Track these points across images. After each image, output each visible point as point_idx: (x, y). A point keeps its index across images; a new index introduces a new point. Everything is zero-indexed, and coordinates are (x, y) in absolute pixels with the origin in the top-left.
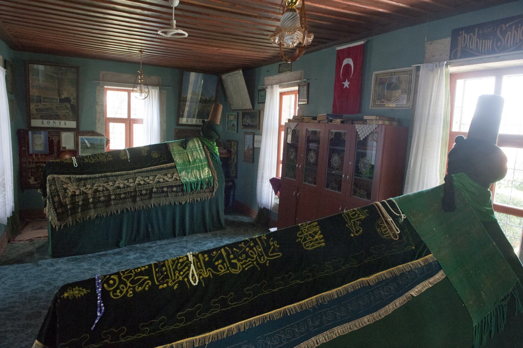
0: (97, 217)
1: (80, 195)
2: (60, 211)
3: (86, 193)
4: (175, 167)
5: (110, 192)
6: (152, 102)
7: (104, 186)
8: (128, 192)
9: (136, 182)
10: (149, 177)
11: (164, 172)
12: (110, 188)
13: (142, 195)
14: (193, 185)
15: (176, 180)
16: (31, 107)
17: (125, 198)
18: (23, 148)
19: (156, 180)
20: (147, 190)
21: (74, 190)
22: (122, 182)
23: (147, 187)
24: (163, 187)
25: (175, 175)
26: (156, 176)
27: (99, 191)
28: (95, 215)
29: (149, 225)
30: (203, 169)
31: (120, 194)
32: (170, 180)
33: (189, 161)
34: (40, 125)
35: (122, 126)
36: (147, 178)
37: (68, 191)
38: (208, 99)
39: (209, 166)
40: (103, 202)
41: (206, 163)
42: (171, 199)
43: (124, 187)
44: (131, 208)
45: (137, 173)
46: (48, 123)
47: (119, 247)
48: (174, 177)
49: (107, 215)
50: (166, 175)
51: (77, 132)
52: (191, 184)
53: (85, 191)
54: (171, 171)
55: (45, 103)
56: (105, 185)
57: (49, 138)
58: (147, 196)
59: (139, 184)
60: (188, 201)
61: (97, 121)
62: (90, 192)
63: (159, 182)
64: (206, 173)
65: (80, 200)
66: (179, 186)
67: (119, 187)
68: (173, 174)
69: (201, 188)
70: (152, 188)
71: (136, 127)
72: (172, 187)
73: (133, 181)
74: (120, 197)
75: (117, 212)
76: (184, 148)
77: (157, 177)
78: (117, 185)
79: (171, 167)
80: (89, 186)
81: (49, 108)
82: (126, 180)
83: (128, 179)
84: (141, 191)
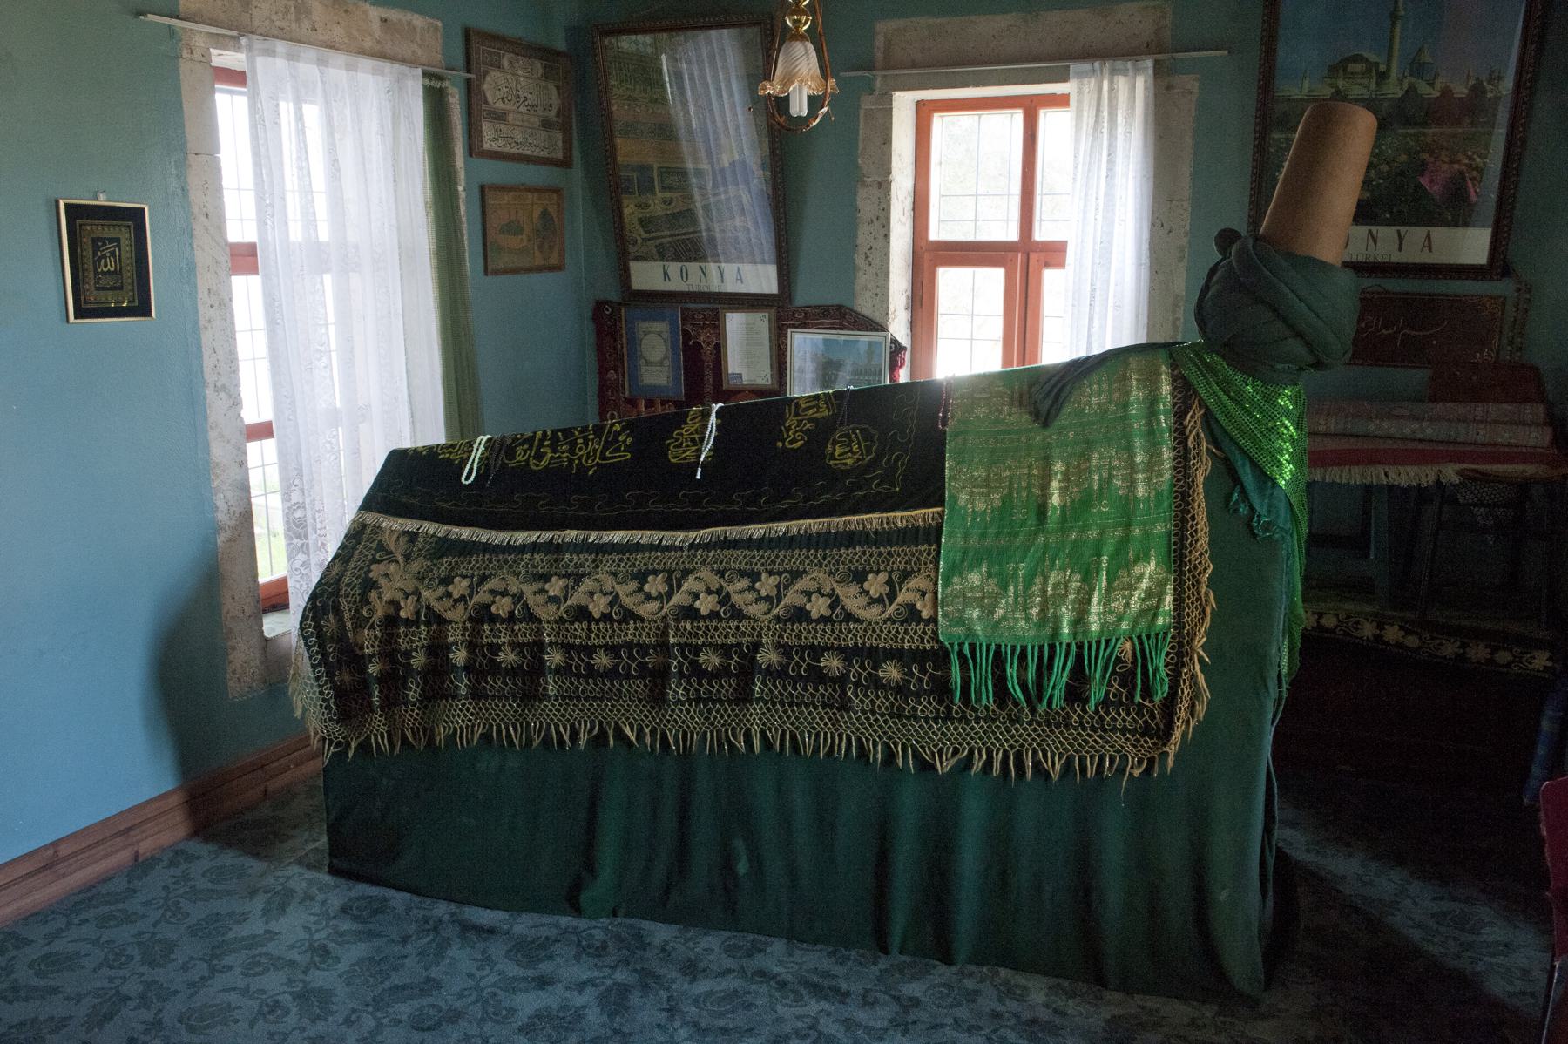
0: (486, 738)
1: (416, 623)
2: (345, 677)
3: (441, 621)
4: (933, 534)
5: (539, 632)
6: (1112, 146)
7: (518, 598)
8: (629, 645)
9: (678, 598)
10: (755, 577)
11: (852, 557)
12: (546, 612)
13: (698, 671)
14: (1012, 672)
15: (912, 614)
16: (626, 211)
17: (611, 674)
18: (612, 375)
19: (792, 598)
20: (725, 650)
21: (399, 596)
22: (609, 583)
23: (728, 633)
24: (817, 651)
25: (913, 583)
26: (797, 575)
27: (493, 619)
28: (479, 731)
29: (739, 844)
30: (1122, 562)
31: (590, 651)
32: (872, 614)
33: (1042, 510)
34: (659, 285)
35: (992, 280)
36: (745, 583)
37: (373, 594)
38: (1461, 91)
39: (1178, 557)
40: (514, 671)
41: (1159, 529)
42: (863, 724)
43: (606, 617)
44: (640, 731)
45: (707, 546)
46: (685, 275)
47: (577, 910)
48: (902, 598)
49: (530, 741)
50: (859, 577)
51: (783, 311)
52: (999, 661)
53: (437, 606)
54: (901, 556)
55: (668, 195)
56: (528, 590)
57: (686, 333)
58: (728, 687)
59: (689, 613)
60: (978, 764)
61: (860, 260)
62: (457, 615)
63: (800, 615)
64: (1126, 601)
65: (414, 644)
66: (920, 657)
67: (582, 613)
68: (906, 575)
69: (1076, 694)
70: (756, 646)
71: (1053, 281)
72: (875, 656)
73: (664, 588)
74: (590, 667)
75: (574, 735)
76: (1036, 415)
77: (801, 584)
78: (578, 598)
79: (912, 535)
80: (460, 587)
81: (681, 212)
82: (634, 577)
83: (642, 577)
84: (696, 650)
